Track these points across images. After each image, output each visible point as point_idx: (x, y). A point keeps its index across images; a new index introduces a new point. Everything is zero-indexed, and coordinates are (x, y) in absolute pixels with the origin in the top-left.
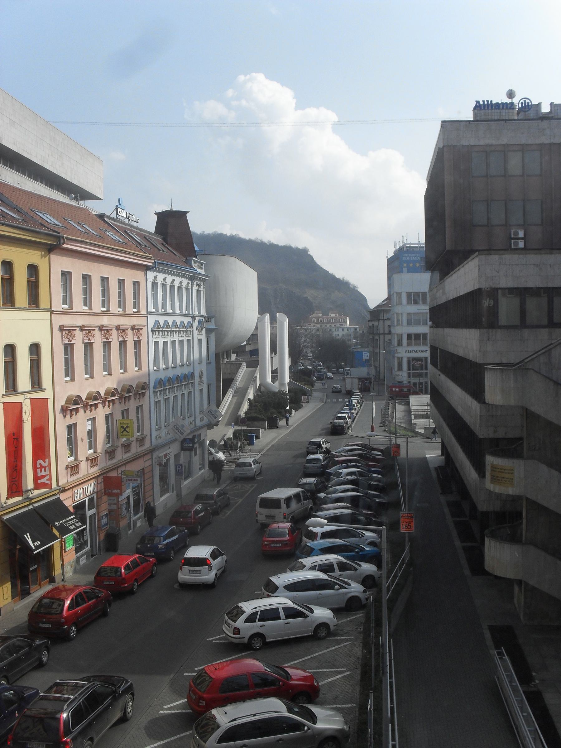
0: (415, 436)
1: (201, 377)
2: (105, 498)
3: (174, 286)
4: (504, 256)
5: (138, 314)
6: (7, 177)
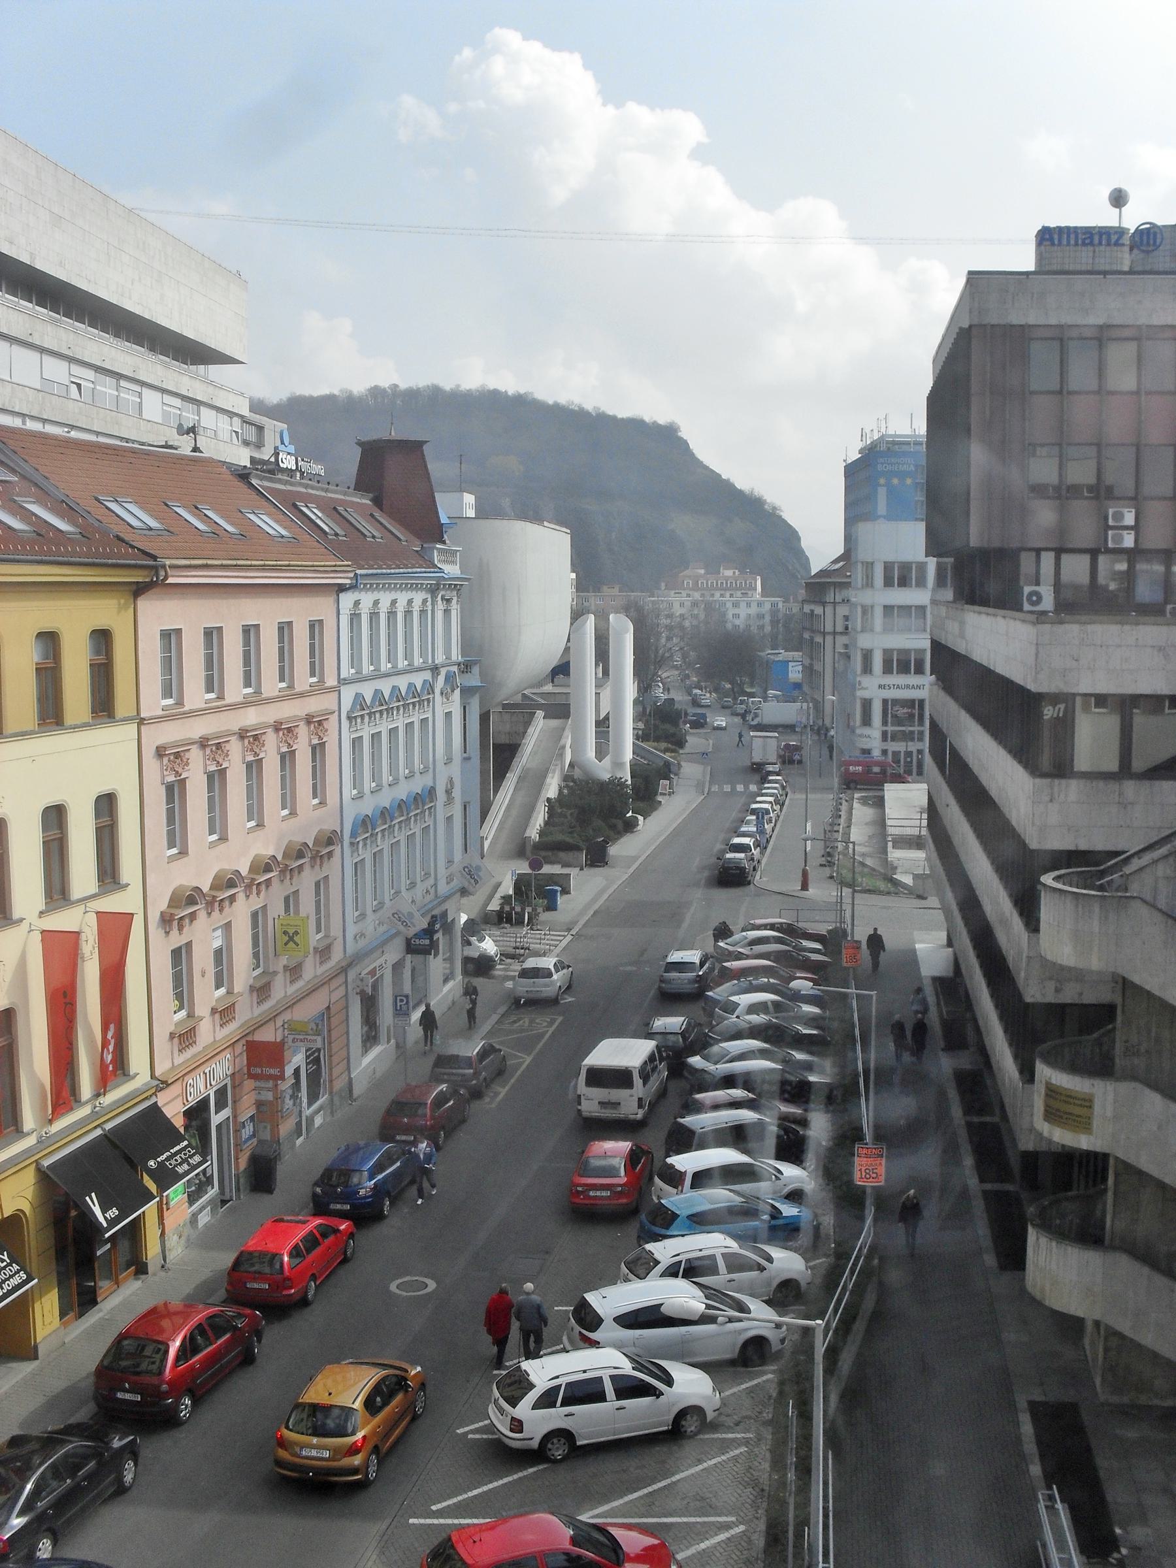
0: (892, 889)
1: (448, 792)
2: (249, 1084)
3: (396, 612)
4: (1090, 628)
5: (320, 688)
6: (46, 336)
